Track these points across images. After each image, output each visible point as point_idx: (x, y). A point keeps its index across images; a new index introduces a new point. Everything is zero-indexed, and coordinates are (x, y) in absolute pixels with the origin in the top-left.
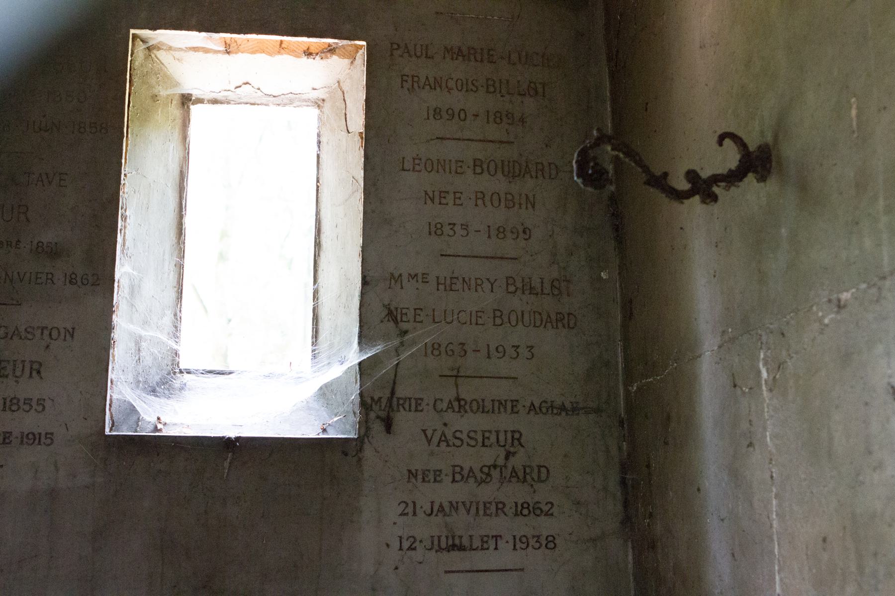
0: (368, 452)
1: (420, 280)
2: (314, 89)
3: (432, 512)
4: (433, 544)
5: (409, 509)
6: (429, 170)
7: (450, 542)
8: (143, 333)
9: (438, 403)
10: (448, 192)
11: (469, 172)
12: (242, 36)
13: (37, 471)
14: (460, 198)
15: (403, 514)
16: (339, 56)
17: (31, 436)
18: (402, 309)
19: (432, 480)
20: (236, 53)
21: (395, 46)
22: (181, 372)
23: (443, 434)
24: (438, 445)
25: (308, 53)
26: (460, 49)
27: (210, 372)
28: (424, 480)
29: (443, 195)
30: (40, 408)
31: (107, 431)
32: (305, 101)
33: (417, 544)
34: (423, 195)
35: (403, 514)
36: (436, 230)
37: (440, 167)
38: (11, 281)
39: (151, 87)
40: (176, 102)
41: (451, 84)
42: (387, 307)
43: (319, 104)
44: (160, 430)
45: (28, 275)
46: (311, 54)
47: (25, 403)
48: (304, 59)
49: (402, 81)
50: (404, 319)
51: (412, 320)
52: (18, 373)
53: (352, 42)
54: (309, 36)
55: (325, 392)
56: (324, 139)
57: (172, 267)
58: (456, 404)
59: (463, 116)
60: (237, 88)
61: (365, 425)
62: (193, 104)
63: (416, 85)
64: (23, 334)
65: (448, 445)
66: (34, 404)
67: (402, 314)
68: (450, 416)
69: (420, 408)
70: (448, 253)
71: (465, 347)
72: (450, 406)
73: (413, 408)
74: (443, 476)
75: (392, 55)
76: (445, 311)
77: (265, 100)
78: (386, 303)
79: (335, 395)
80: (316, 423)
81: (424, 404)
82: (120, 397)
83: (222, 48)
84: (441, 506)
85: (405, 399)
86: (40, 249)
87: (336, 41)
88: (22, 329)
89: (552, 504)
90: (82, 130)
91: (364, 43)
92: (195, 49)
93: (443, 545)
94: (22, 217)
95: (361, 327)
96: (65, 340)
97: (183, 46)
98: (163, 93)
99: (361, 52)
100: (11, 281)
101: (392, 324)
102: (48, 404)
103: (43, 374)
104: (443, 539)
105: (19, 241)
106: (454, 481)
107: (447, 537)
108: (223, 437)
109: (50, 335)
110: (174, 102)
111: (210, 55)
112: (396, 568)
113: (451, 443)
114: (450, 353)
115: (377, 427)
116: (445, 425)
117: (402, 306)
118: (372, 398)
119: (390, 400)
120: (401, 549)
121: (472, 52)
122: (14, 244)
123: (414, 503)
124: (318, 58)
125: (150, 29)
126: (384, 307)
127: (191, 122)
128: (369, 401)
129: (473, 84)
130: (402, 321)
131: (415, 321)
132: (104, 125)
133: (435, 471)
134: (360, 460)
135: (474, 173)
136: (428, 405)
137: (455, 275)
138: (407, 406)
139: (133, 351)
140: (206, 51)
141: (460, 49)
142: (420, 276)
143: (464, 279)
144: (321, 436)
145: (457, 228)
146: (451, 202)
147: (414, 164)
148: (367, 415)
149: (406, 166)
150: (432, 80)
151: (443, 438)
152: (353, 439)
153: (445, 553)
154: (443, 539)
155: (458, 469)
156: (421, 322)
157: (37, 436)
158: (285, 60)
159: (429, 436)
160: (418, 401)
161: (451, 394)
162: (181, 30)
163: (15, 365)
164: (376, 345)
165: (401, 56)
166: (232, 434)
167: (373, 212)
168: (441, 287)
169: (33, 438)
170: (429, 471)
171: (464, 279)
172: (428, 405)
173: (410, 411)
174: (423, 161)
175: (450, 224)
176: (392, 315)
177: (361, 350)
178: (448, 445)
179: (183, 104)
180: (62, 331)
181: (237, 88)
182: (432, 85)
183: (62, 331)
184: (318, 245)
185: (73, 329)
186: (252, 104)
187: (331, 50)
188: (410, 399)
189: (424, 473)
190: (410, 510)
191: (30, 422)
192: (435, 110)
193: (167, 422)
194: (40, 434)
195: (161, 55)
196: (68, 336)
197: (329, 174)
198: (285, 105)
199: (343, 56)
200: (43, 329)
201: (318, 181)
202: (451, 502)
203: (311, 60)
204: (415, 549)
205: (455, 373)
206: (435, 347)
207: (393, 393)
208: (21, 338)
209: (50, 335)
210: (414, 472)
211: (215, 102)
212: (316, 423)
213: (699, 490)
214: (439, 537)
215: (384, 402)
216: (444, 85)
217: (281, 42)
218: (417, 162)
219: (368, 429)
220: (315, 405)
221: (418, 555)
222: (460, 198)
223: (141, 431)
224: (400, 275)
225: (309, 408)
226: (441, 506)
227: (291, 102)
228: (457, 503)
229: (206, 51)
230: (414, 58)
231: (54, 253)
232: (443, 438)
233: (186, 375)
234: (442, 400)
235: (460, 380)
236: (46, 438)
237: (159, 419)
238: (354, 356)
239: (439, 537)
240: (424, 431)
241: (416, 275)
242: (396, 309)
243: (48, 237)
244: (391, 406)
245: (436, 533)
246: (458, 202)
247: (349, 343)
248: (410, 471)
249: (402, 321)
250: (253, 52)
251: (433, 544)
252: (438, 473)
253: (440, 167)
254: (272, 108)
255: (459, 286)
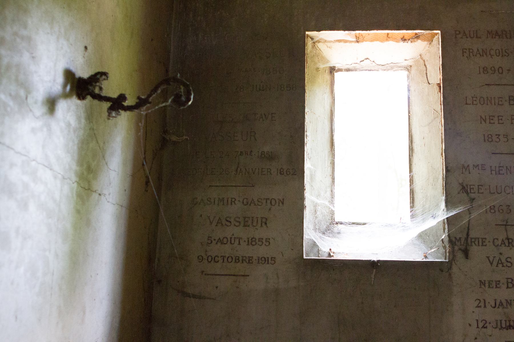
0: (455, 269)
1: (480, 168)
2: (406, 60)
3: (495, 305)
4: (497, 324)
5: (482, 304)
6: (482, 103)
7: (508, 324)
8: (319, 202)
9: (496, 240)
10: (494, 116)
11: (507, 104)
12: (368, 32)
13: (267, 278)
14: (502, 119)
15: (478, 307)
16: (422, 40)
17: (263, 259)
18: (470, 185)
19: (495, 287)
20: (362, 42)
21: (458, 32)
22: (337, 224)
23: (500, 259)
24: (497, 266)
25: (404, 39)
26: (497, 32)
27: (353, 223)
28: (489, 287)
29: (491, 118)
30: (267, 244)
31: (305, 257)
32: (400, 67)
33: (487, 324)
34: (479, 118)
35: (478, 307)
36: (489, 138)
37: (488, 102)
38: (248, 173)
39: (315, 64)
40: (327, 71)
41: (493, 52)
42: (461, 184)
43: (408, 68)
44: (333, 256)
45: (257, 170)
46: (405, 40)
47: (259, 241)
48: (401, 43)
49: (463, 52)
50: (472, 191)
51: (477, 191)
52: (255, 224)
53: (432, 32)
54: (407, 29)
55: (422, 236)
56: (412, 89)
57: (329, 164)
58: (506, 242)
59: (500, 71)
60: (361, 61)
61: (452, 253)
62: (336, 72)
63: (471, 54)
64: (256, 203)
65: (503, 266)
66: (264, 241)
67: (470, 189)
68: (503, 249)
69: (484, 244)
70: (497, 152)
71: (510, 208)
72: (503, 242)
73: (481, 244)
74: (501, 284)
75: (456, 38)
76: (496, 187)
77: (377, 68)
78: (461, 182)
79: (428, 236)
80: (420, 253)
81: (487, 241)
82: (308, 237)
83: (355, 40)
84: (501, 302)
85: (475, 239)
86: (263, 156)
87: (422, 31)
88: (255, 200)
89: (486, 321)
90: (282, 89)
91: (439, 32)
92: (339, 41)
93: (504, 326)
94: (253, 138)
95: (446, 196)
96: (279, 206)
97: (332, 40)
98: (321, 66)
99: (436, 37)
100: (248, 173)
101: (465, 194)
102: (271, 241)
103: (268, 225)
104: (503, 322)
105: (252, 151)
106: (508, 287)
107: (506, 321)
108: (370, 260)
109: (271, 202)
110: (327, 71)
111: (348, 44)
112: (476, 339)
113: (505, 265)
114: (501, 211)
115: (460, 255)
116: (501, 254)
117: (470, 184)
118: (455, 238)
119: (466, 239)
120: (478, 327)
121: (504, 33)
122: (249, 153)
123: (485, 300)
124: (409, 42)
125: (317, 31)
126: (458, 185)
127: (335, 84)
128: (454, 240)
129: (506, 52)
130: (471, 192)
131: (478, 193)
132: (294, 86)
133: (496, 281)
134: (450, 275)
135: (510, 104)
136: (489, 242)
137: (501, 165)
138: (477, 243)
139: (313, 211)
140: (346, 41)
141: (497, 32)
142: (480, 166)
143: (507, 167)
144: (424, 260)
145: (501, 137)
146: (497, 122)
147: (473, 101)
148: (453, 248)
149: (468, 102)
150: (481, 51)
151: (500, 262)
152: (446, 262)
153: (505, 330)
154: (503, 322)
155: (510, 281)
156: (483, 193)
157: (267, 259)
158: (391, 44)
159: (491, 261)
160: (484, 240)
161: (502, 236)
162: (334, 30)
163: (252, 220)
164: (458, 207)
165: (462, 38)
166: (375, 258)
167: (450, 129)
168: (494, 172)
169: (265, 260)
170: (492, 281)
171: (507, 167)
172: (489, 242)
173: (479, 245)
174: (478, 99)
175: (496, 135)
176: (464, 189)
177: (447, 210)
178: (503, 266)
179: (331, 72)
180: (277, 201)
181: (361, 61)
182: (481, 54)
183: (277, 201)
184: (411, 150)
185: (283, 199)
186: (369, 70)
187: (417, 37)
188: (478, 238)
189: (489, 283)
190: (482, 304)
191: (262, 251)
192: (483, 69)
193: (335, 252)
194: (268, 258)
195: (320, 45)
196: (281, 204)
197: (416, 109)
198: (388, 70)
199: (424, 40)
200: (267, 199)
201: (409, 113)
202: (506, 300)
203: (405, 44)
204: (486, 327)
205: (505, 223)
206: (492, 208)
207: (468, 235)
208: (255, 205)
209: (271, 202)
210: (483, 282)
211: (348, 70)
212: (420, 253)
213: (86, 48)
214: (501, 321)
215: (463, 240)
216: (488, 53)
217: (388, 34)
218: (474, 99)
219: (454, 256)
220: (417, 242)
221: (489, 331)
222: (502, 119)
223: (322, 257)
224: (468, 166)
225: (414, 244)
226: (501, 302)
227: (392, 68)
228: (511, 300)
229: (346, 41)
230: (469, 39)
231: (271, 157)
232: (500, 262)
233: (339, 226)
234: (497, 239)
235: (508, 227)
236: (271, 260)
237: (330, 250)
238: (442, 214)
239: (501, 321)
240: (488, 257)
241: (478, 165)
242: (467, 185)
243: (267, 149)
244: (467, 243)
245: (499, 318)
246: (500, 122)
247: (437, 206)
248: (480, 281)
249: (471, 192)
250: (372, 41)
251: (497, 324)
252: (498, 283)
253: (488, 102)
254: (380, 71)
255: (504, 171)
